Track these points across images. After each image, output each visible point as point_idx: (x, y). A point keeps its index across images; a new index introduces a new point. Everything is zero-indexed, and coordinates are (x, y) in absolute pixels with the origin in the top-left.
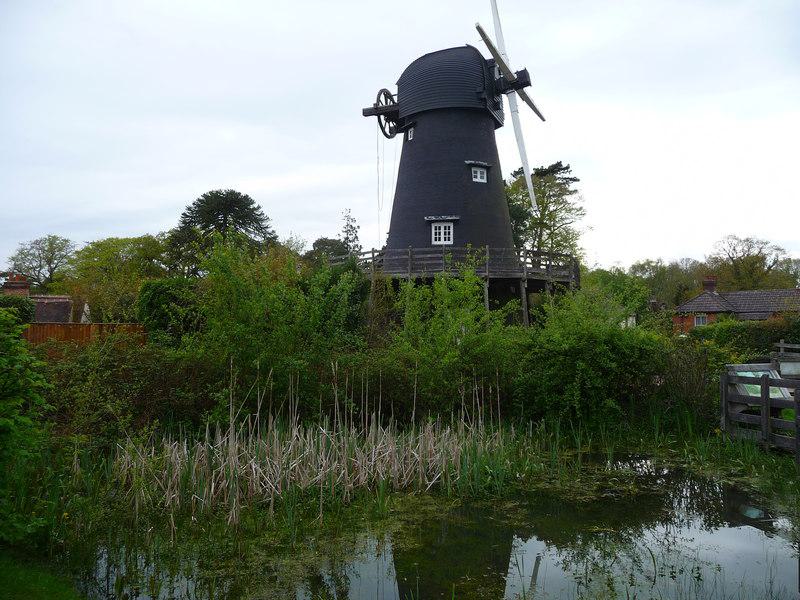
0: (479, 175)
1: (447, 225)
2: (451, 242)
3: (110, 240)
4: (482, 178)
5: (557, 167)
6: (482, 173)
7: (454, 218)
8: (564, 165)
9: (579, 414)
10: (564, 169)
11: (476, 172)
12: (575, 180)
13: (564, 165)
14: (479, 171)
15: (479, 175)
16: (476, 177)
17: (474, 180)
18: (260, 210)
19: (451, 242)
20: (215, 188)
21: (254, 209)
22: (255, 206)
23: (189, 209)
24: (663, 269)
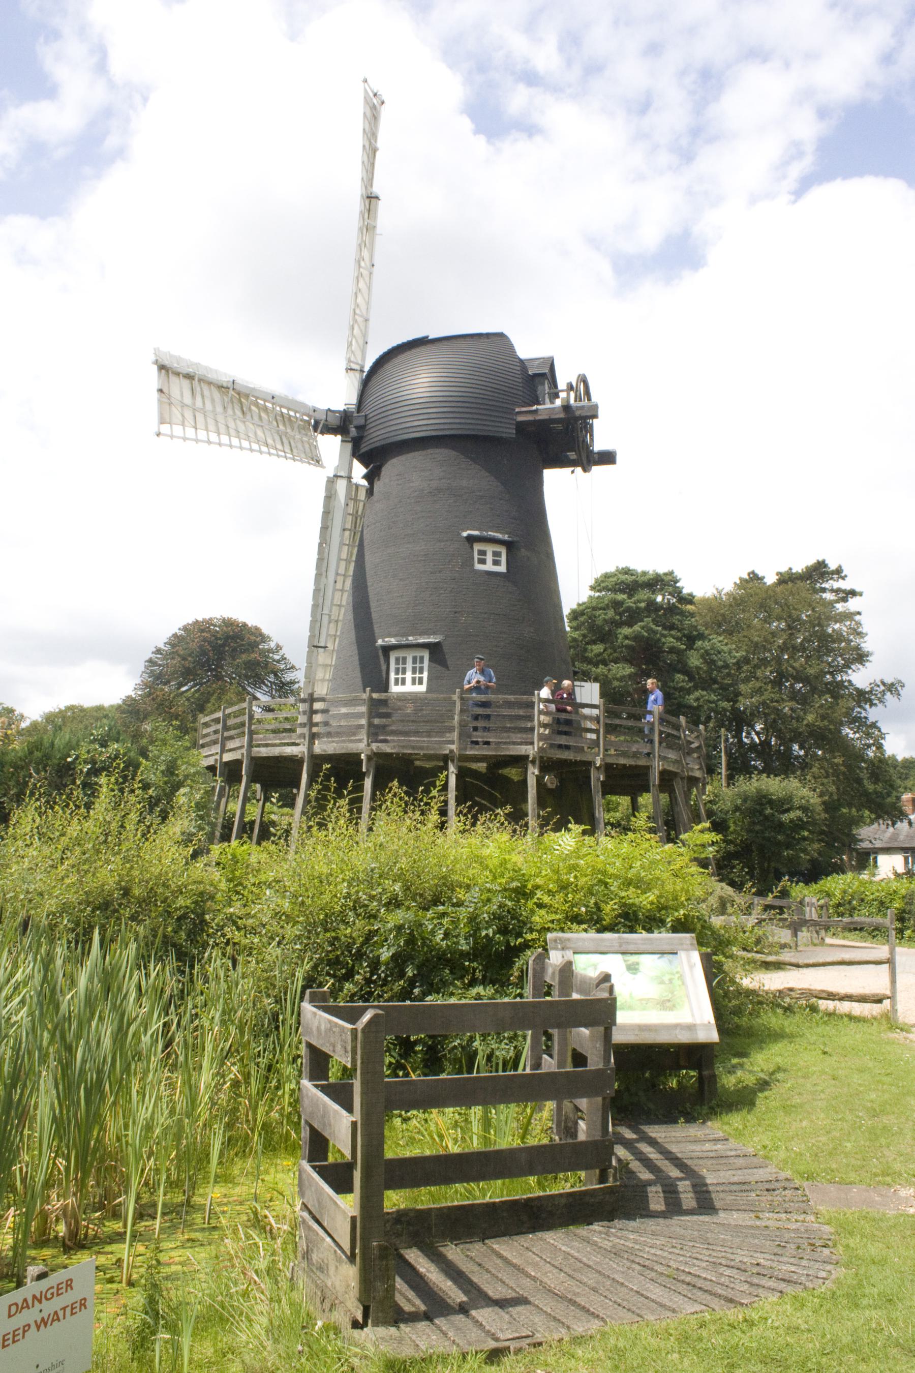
0: (489, 558)
1: (418, 653)
2: (423, 688)
3: (71, 708)
4: (496, 563)
5: (819, 571)
6: (496, 554)
7: (432, 639)
8: (833, 566)
9: (277, 939)
10: (833, 573)
11: (482, 553)
12: (853, 593)
13: (833, 566)
14: (490, 549)
15: (489, 558)
16: (482, 561)
17: (479, 567)
18: (281, 653)
19: (423, 688)
20: (202, 614)
21: (270, 651)
22: (272, 645)
23: (158, 651)
24: (214, 634)
